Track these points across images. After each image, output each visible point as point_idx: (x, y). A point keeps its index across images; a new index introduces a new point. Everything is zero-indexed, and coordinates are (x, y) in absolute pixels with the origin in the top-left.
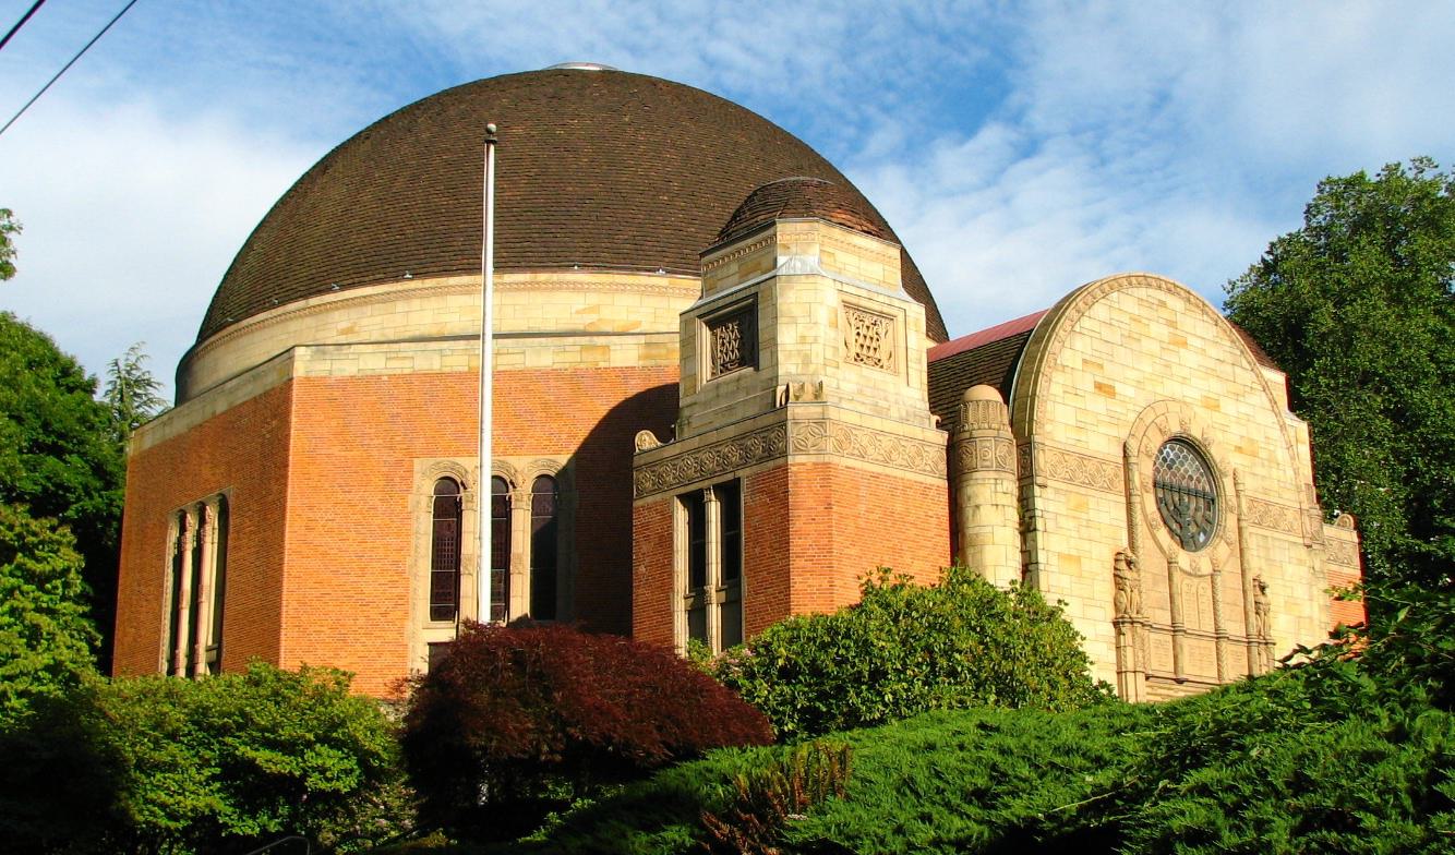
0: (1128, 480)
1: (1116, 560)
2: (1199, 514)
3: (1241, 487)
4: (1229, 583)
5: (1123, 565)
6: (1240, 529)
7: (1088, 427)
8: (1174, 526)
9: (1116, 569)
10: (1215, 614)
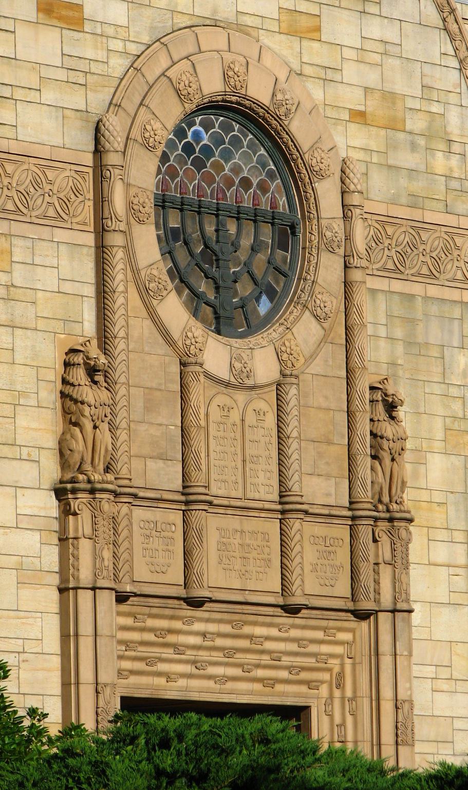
0: (101, 201)
1: (67, 365)
2: (262, 257)
3: (355, 199)
4: (320, 403)
5: (79, 376)
6: (347, 284)
7: (19, 94)
8: (203, 287)
9: (64, 381)
10: (280, 463)
